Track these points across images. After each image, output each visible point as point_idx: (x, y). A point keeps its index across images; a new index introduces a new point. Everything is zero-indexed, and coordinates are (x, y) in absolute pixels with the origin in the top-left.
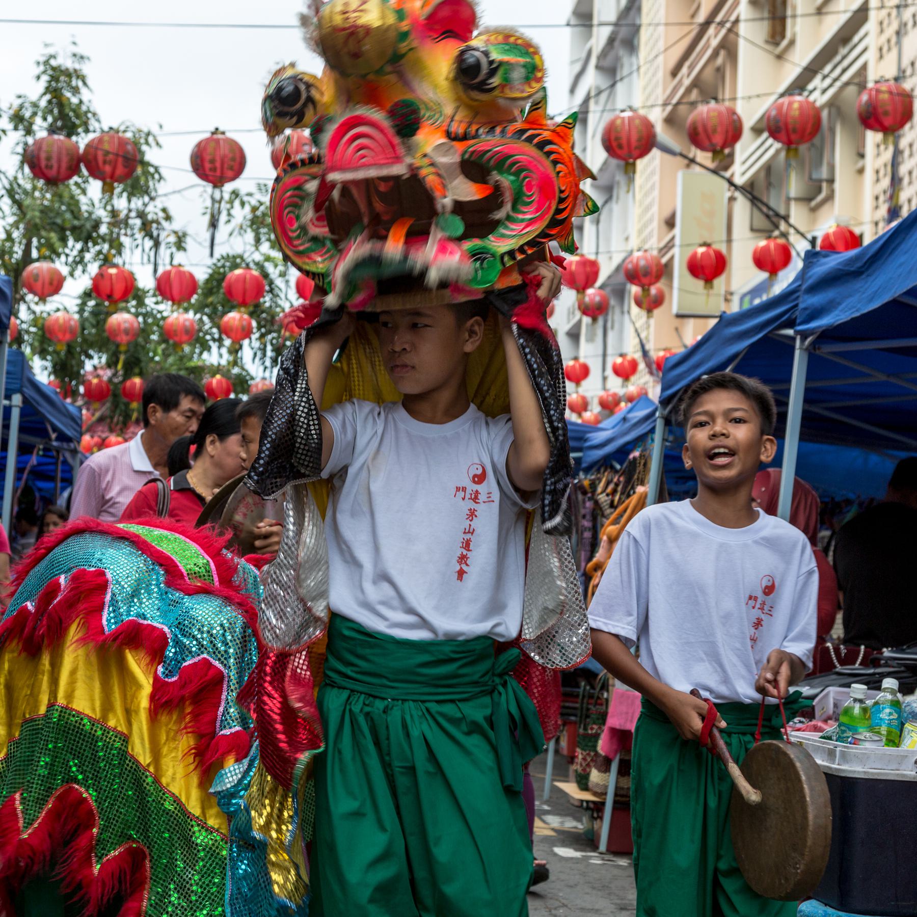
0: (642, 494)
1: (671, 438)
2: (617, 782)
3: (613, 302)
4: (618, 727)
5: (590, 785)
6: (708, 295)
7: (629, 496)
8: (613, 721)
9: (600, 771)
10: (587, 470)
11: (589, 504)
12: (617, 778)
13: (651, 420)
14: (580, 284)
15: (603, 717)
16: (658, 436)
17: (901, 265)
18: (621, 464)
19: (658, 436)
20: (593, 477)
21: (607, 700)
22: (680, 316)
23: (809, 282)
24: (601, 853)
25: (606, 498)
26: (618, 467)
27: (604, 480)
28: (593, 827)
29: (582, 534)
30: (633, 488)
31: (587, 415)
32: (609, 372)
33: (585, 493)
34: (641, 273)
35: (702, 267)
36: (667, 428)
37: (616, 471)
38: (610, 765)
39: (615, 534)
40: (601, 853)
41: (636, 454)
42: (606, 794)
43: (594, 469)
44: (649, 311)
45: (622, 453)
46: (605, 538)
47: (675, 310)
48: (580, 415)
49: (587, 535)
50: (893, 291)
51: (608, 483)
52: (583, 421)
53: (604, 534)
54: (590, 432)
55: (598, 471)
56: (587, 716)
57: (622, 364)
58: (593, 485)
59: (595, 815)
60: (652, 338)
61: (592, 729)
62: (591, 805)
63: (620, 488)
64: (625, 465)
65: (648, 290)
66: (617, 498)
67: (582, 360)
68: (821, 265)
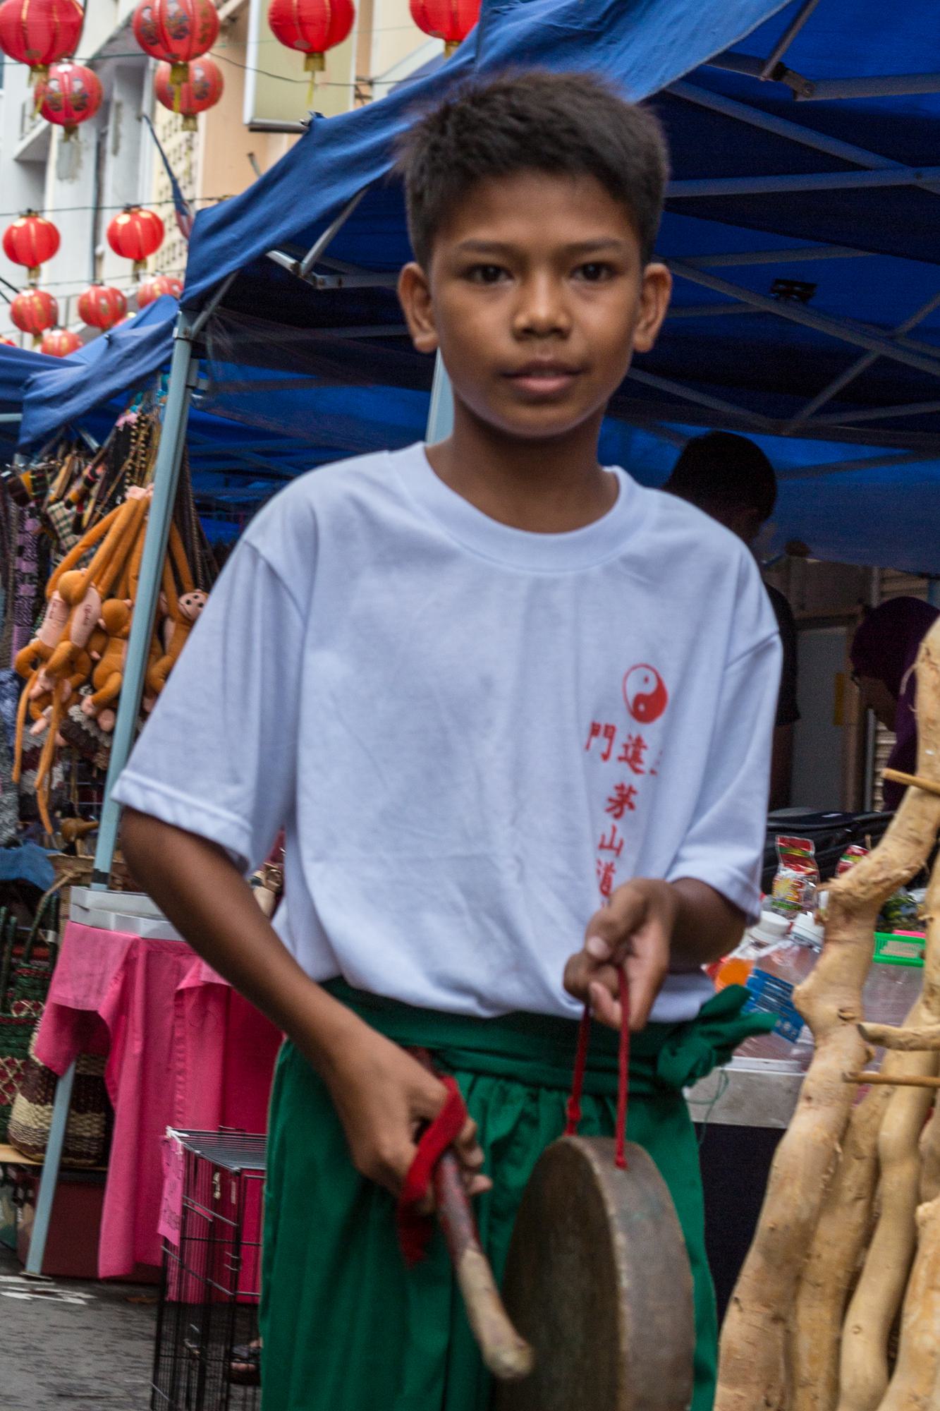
0: (138, 502)
1: (204, 385)
2: (68, 1124)
3: (118, 95)
4: (71, 1005)
5: (12, 1128)
6: (314, 86)
7: (112, 505)
8: (64, 992)
9: (31, 1099)
10: (30, 451)
11: (32, 525)
12: (69, 1115)
13: (163, 345)
14: (38, 51)
15: (42, 984)
16: (176, 379)
17: (678, 19)
18: (100, 441)
19: (176, 379)
20: (40, 466)
21: (55, 947)
22: (255, 128)
23: (492, 53)
24: (29, 1278)
25: (67, 512)
26: (94, 444)
27: (63, 471)
28: (16, 1223)
29: (16, 587)
30: (121, 490)
31: (53, 337)
32: (104, 247)
33: (22, 500)
34: (170, 31)
35: (302, 22)
36: (196, 362)
37: (90, 454)
38: (54, 1088)
39: (77, 587)
40: (29, 1278)
41: (131, 417)
42: (43, 1149)
43: (45, 449)
44: (189, 115)
45: (104, 412)
46: (56, 596)
47: (247, 117)
48: (37, 335)
49: (26, 590)
50: (658, 76)
51: (72, 479)
52: (45, 350)
53: (54, 589)
54: (39, 369)
55: (53, 454)
56: (11, 983)
57: (130, 226)
58: (41, 483)
59: (21, 1194)
60: (198, 173)
61: (20, 1008)
62: (13, 1174)
63: (94, 491)
64: (107, 443)
65: (185, 68)
66: (88, 512)
67: (48, 217)
68: (516, 19)
